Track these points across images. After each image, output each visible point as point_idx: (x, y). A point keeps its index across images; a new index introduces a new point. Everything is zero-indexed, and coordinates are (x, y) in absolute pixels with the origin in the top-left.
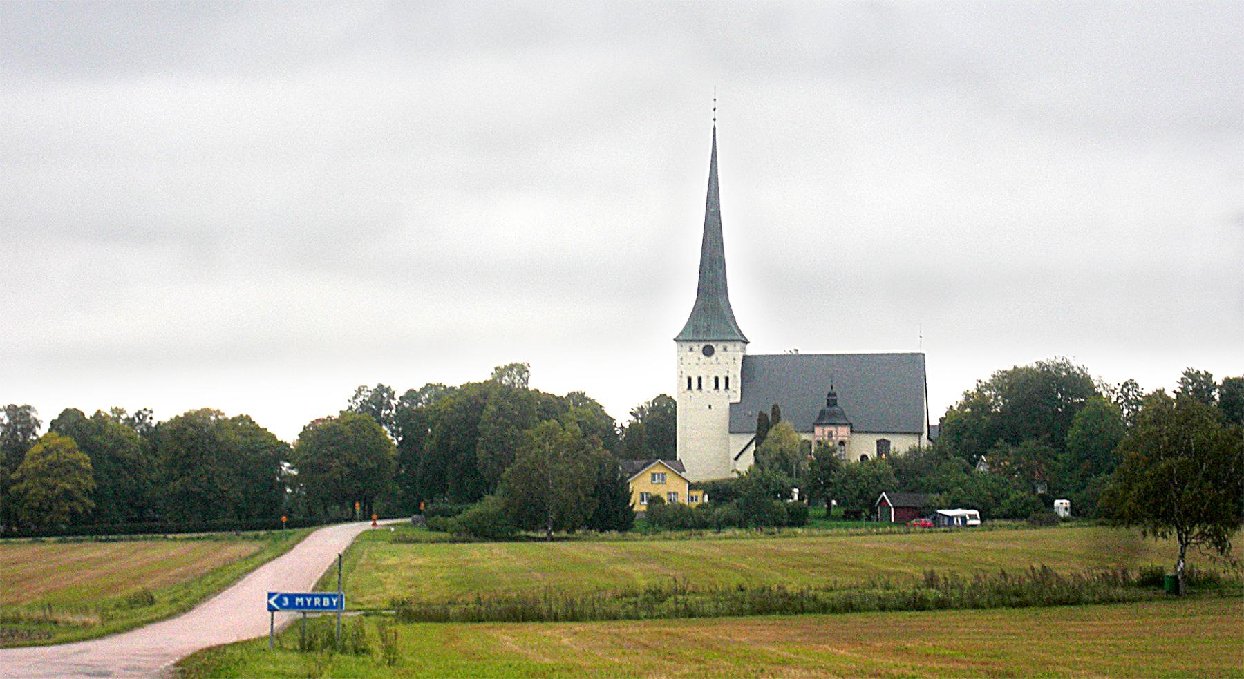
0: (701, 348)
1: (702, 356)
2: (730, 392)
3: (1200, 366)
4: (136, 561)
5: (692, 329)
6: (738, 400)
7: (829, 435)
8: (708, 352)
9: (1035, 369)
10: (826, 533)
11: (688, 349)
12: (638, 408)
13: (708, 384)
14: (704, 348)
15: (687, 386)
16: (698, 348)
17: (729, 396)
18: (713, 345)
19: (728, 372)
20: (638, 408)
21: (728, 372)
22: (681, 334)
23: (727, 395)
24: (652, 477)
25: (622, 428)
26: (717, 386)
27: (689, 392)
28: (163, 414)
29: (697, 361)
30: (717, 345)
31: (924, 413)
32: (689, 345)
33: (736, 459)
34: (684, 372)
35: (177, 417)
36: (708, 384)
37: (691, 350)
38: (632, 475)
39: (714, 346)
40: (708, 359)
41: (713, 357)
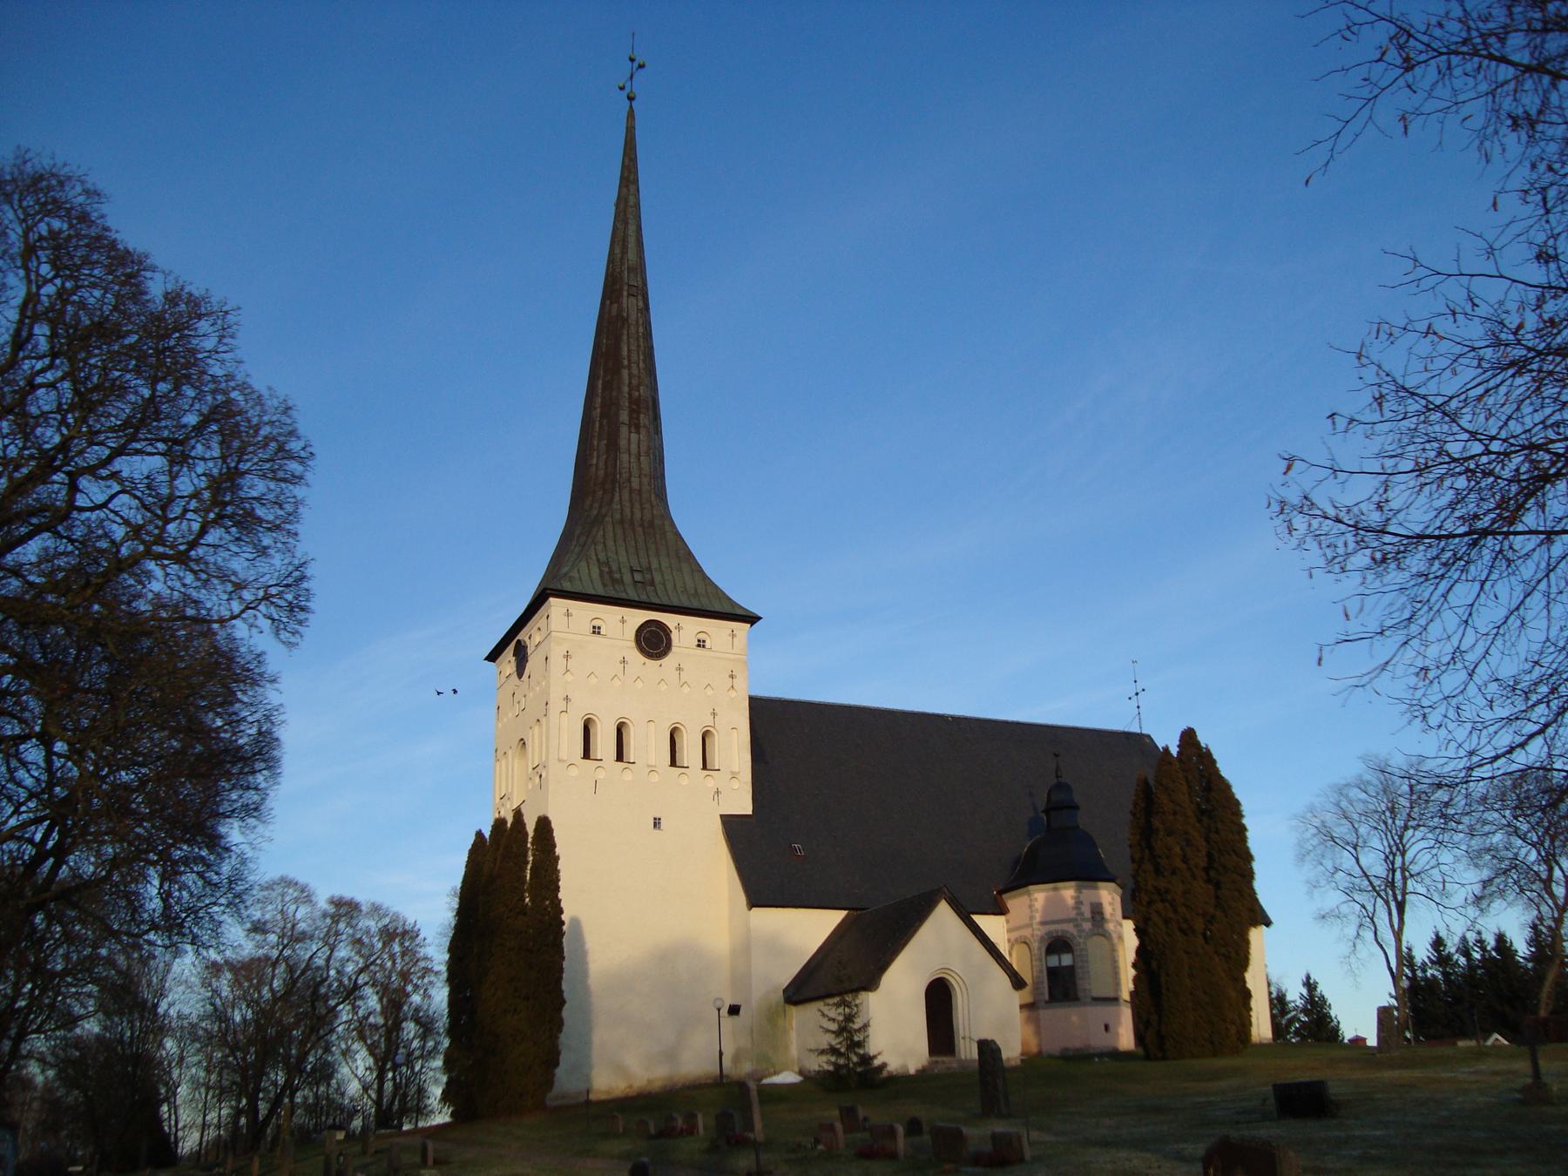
1: (636, 657)
13: (648, 745)
36: (648, 745)
41: (669, 661)
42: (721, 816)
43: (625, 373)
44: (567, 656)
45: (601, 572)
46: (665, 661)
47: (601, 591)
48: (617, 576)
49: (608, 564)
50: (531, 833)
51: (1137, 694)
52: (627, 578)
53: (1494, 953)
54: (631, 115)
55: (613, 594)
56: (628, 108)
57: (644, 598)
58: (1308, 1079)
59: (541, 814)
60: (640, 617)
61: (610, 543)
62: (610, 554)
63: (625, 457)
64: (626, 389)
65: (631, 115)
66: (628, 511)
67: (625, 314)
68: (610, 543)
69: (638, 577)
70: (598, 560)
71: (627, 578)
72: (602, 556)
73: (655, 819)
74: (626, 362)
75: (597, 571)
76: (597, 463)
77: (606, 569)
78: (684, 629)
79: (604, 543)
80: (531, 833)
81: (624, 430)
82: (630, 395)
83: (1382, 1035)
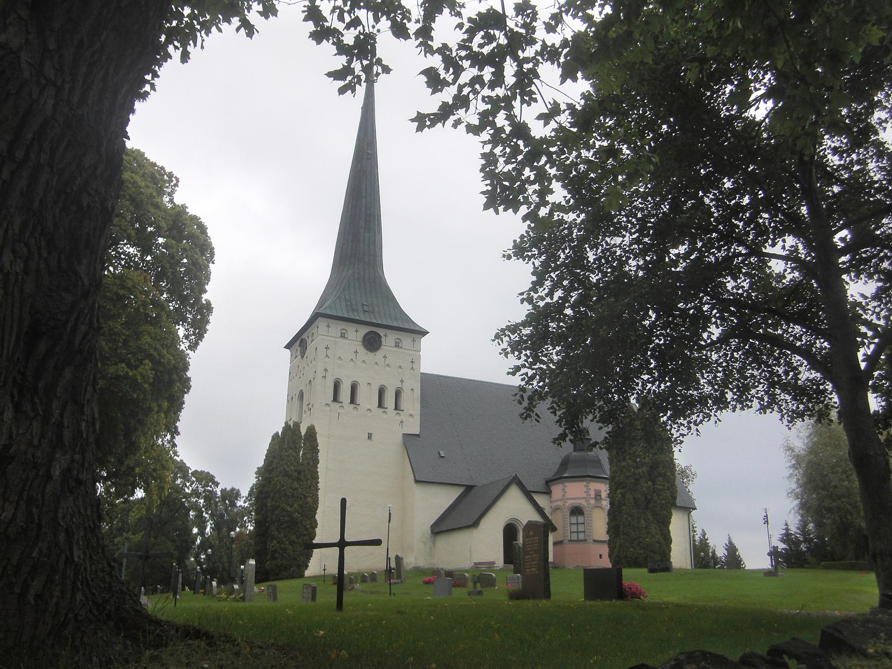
0: (360, 338)
1: (362, 350)
2: (404, 416)
4: (154, 339)
5: (343, 304)
6: (417, 431)
7: (596, 495)
8: (372, 343)
9: (165, 482)
13: (367, 397)
14: (366, 335)
16: (356, 334)
17: (402, 422)
19: (402, 381)
21: (402, 381)
23: (399, 418)
24: (401, 575)
25: (140, 488)
27: (337, 405)
30: (386, 335)
32: (342, 325)
33: (377, 542)
36: (367, 397)
37: (343, 336)
38: (373, 577)
41: (380, 353)
45: (347, 305)
47: (346, 315)
48: (355, 307)
60: (364, 330)
69: (366, 308)
71: (360, 308)
72: (348, 298)
77: (349, 304)
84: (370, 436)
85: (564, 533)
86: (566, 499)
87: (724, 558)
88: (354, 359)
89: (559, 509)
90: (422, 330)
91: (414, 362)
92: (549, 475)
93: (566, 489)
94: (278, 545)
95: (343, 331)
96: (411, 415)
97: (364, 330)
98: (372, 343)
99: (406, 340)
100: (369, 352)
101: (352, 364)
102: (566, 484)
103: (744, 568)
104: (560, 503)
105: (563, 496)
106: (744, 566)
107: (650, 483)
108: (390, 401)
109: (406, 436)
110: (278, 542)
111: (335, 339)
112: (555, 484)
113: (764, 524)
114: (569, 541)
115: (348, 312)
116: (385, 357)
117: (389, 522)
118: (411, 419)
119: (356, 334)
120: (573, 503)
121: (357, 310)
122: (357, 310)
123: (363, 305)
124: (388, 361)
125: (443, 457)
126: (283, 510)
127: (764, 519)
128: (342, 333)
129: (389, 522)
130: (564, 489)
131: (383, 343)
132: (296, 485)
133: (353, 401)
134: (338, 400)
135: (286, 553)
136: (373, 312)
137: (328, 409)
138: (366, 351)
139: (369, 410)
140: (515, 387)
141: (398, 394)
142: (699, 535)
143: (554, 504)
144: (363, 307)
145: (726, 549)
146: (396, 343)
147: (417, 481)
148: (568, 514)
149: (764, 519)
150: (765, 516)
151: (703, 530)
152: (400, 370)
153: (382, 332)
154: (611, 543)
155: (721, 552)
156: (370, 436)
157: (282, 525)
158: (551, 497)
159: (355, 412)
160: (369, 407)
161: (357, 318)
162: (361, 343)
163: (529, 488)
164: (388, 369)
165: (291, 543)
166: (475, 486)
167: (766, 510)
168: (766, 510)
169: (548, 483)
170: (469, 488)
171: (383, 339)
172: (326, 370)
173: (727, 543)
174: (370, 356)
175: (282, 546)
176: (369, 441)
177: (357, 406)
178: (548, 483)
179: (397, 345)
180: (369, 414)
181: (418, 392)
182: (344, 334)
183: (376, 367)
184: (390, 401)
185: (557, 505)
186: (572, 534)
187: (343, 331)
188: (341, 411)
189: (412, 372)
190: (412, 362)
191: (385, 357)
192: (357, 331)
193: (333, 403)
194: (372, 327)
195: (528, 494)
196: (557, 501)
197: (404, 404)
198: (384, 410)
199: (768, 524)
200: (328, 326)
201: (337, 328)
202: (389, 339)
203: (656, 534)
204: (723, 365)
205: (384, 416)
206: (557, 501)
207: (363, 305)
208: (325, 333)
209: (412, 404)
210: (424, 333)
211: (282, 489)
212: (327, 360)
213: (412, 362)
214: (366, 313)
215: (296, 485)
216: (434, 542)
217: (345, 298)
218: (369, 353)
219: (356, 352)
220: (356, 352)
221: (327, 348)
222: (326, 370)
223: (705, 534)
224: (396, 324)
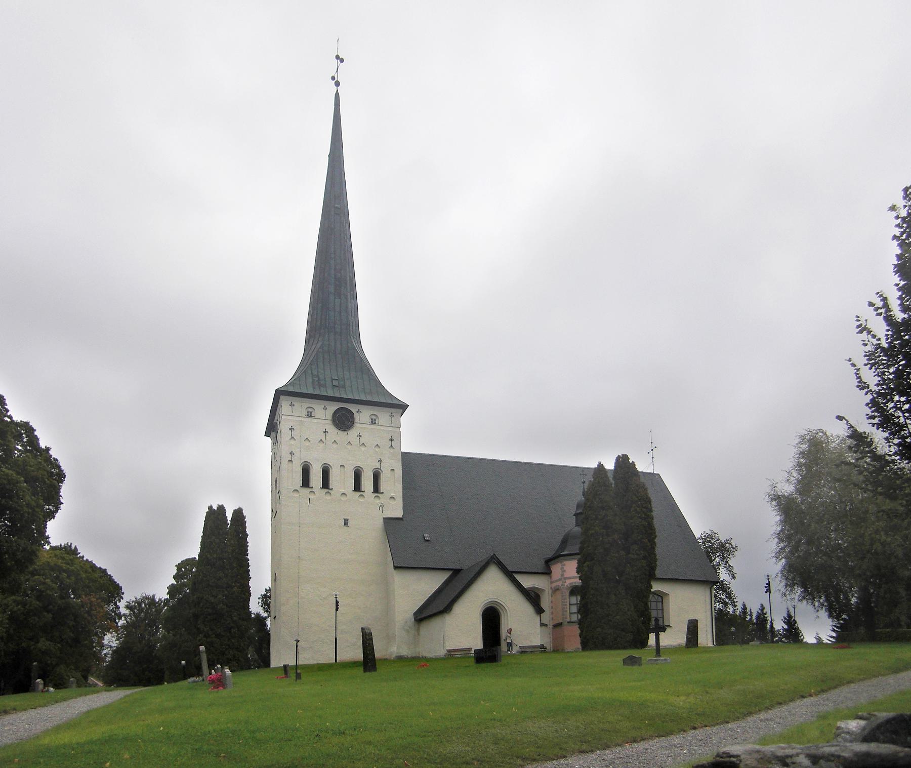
1: (332, 429)
2: (383, 499)
3: (88, 559)
5: (310, 380)
8: (343, 421)
10: (761, 747)
11: (305, 413)
12: (48, 536)
13: (342, 481)
15: (300, 482)
16: (324, 412)
17: (382, 505)
18: (353, 408)
19: (380, 461)
20: (48, 536)
21: (380, 461)
22: (291, 383)
23: (378, 501)
26: (358, 487)
28: (243, 512)
29: (362, 440)
30: (359, 412)
31: (715, 624)
32: (306, 403)
34: (297, 454)
35: (207, 513)
36: (342, 481)
37: (310, 415)
39: (354, 411)
40: (342, 434)
41: (353, 433)
42: (384, 518)
43: (332, 262)
44: (292, 429)
45: (313, 381)
46: (351, 432)
47: (310, 391)
48: (322, 382)
49: (318, 376)
50: (229, 519)
51: (652, 450)
52: (329, 383)
53: (899, 262)
54: (337, 96)
55: (318, 392)
56: (336, 90)
57: (337, 395)
58: (103, 704)
59: (220, 504)
60: (333, 407)
61: (321, 365)
62: (320, 370)
63: (332, 313)
64: (333, 272)
65: (337, 96)
66: (333, 344)
67: (332, 226)
68: (321, 365)
69: (335, 383)
70: (312, 374)
71: (329, 383)
72: (315, 373)
73: (345, 520)
74: (333, 256)
75: (311, 380)
76: (317, 318)
77: (316, 379)
78: (363, 415)
79: (317, 364)
80: (229, 519)
81: (332, 297)
82: (335, 276)
83: (690, 625)
84: (346, 523)
85: (563, 615)
86: (565, 578)
87: (782, 631)
88: (324, 439)
89: (558, 589)
90: (403, 404)
91: (394, 440)
92: (550, 554)
93: (565, 568)
94: (205, 639)
95: (310, 410)
96: (392, 498)
97: (333, 407)
98: (343, 421)
99: (384, 416)
100: (340, 432)
101: (322, 445)
102: (564, 562)
103: (802, 640)
104: (559, 583)
105: (562, 575)
106: (802, 637)
107: (622, 553)
108: (367, 483)
109: (387, 520)
110: (205, 636)
111: (299, 419)
112: (554, 564)
113: (766, 592)
114: (568, 622)
115: (314, 388)
116: (359, 436)
117: (337, 610)
118: (392, 502)
119: (324, 412)
120: (572, 583)
121: (325, 386)
122: (325, 386)
123: (332, 380)
124: (362, 440)
125: (428, 540)
126: (207, 601)
127: (766, 587)
128: (308, 412)
129: (337, 610)
130: (563, 568)
131: (357, 420)
132: (221, 574)
133: (376, 489)
134: (379, 492)
135: (213, 646)
136: (344, 387)
137: (296, 495)
138: (337, 431)
139: (344, 494)
140: (591, 469)
141: (376, 477)
142: (740, 609)
143: (554, 585)
144: (332, 382)
145: (784, 622)
146: (372, 419)
147: (396, 568)
148: (568, 594)
149: (766, 587)
150: (767, 584)
151: (762, 605)
152: (377, 449)
153: (353, 408)
154: (580, 623)
155: (779, 625)
156: (346, 523)
157: (207, 617)
158: (551, 577)
159: (328, 497)
160: (343, 491)
161: (324, 394)
162: (330, 422)
163: (510, 569)
164: (363, 448)
165: (218, 636)
166: (462, 570)
167: (768, 576)
168: (768, 576)
169: (548, 562)
170: (456, 572)
171: (356, 415)
172: (292, 453)
173: (786, 616)
174: (341, 436)
175: (209, 640)
176: (345, 527)
177: (330, 491)
178: (548, 562)
179: (373, 422)
180: (344, 498)
181: (399, 472)
182: (375, 420)
183: (349, 447)
184: (367, 483)
185: (557, 586)
186: (572, 615)
187: (310, 410)
188: (312, 496)
189: (392, 450)
190: (391, 440)
191: (359, 436)
192: (325, 409)
193: (302, 488)
194: (341, 403)
195: (510, 575)
196: (557, 581)
197: (383, 487)
198: (362, 493)
199: (770, 593)
200: (292, 405)
201: (301, 406)
202: (363, 415)
203: (628, 610)
204: (907, 440)
205: (361, 500)
206: (557, 581)
207: (332, 380)
208: (291, 413)
209: (393, 486)
210: (403, 407)
211: (205, 579)
212: (292, 442)
213: (391, 440)
214: (336, 388)
215: (221, 574)
216: (418, 630)
217: (312, 374)
218: (340, 432)
219: (325, 432)
220: (325, 432)
221: (292, 429)
222: (292, 453)
223: (764, 609)
224: (369, 398)
